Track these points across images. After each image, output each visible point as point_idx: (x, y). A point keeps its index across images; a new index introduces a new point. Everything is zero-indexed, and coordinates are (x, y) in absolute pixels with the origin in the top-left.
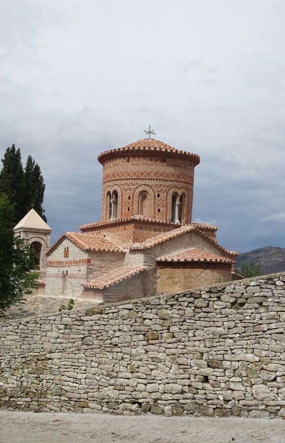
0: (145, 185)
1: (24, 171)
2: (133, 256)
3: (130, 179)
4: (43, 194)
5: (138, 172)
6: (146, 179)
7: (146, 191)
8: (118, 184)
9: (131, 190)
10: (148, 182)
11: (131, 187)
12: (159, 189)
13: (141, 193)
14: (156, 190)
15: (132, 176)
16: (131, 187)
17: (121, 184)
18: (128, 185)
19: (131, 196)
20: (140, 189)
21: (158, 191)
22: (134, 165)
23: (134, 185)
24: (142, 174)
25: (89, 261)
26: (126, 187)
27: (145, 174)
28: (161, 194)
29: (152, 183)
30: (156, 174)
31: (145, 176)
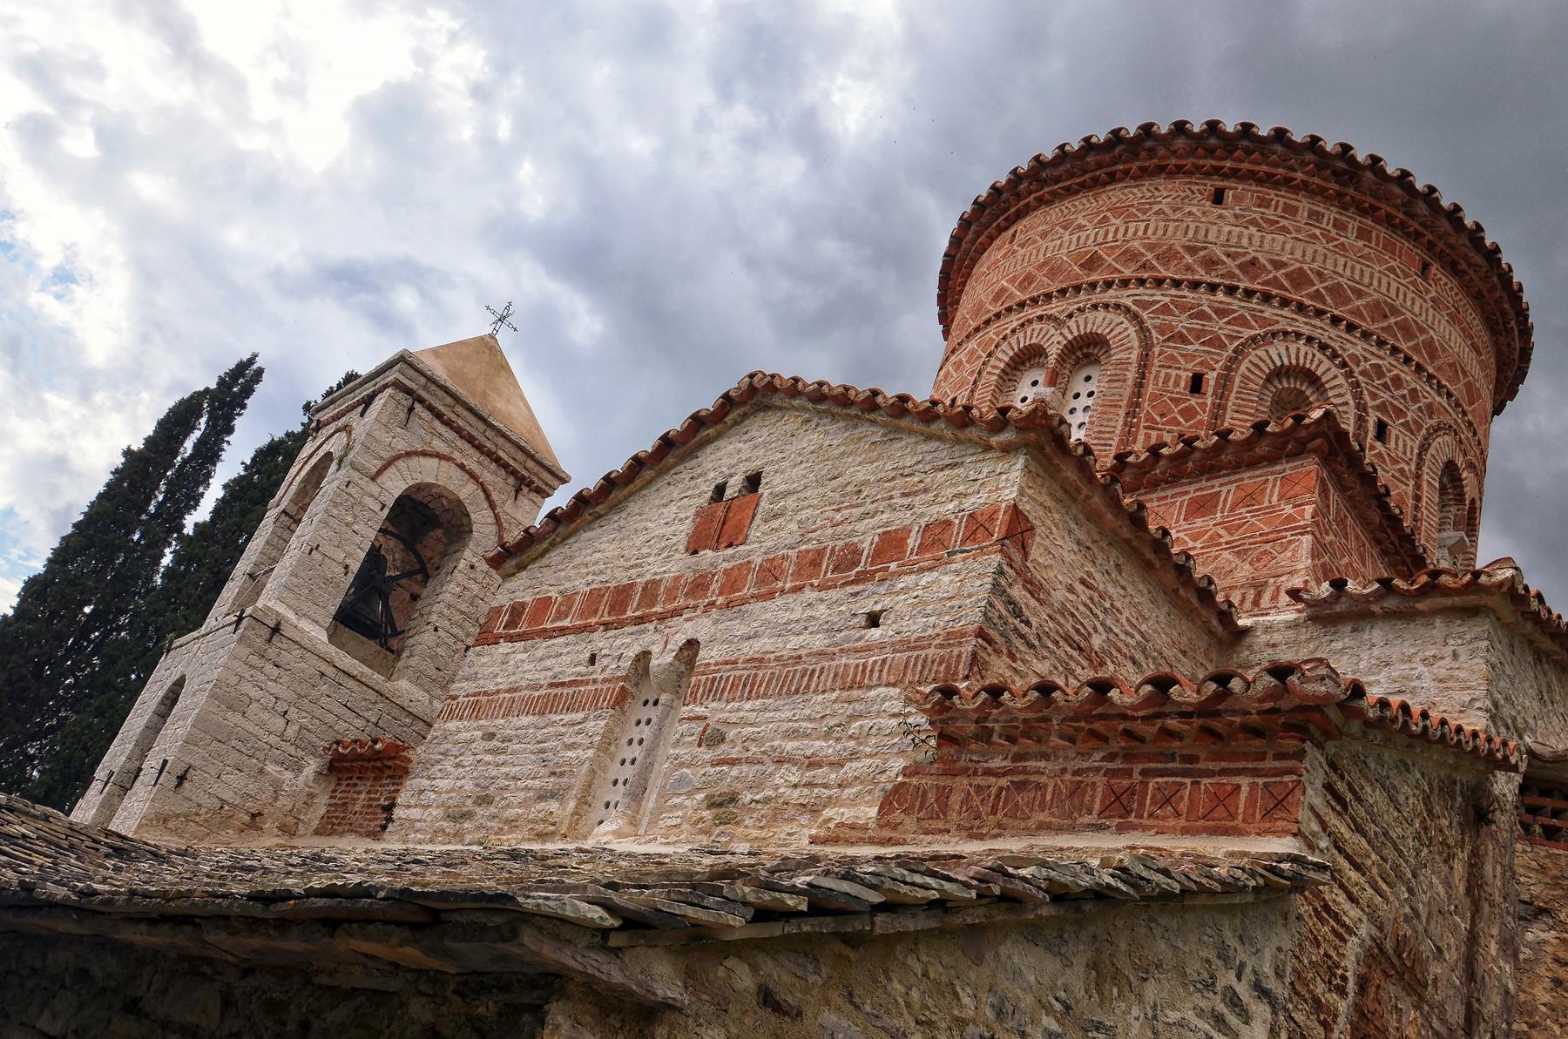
0: (1310, 340)
1: (158, 580)
2: (565, 466)
3: (1213, 288)
4: (61, 557)
5: (1278, 265)
6: (1319, 313)
7: (1312, 378)
8: (1128, 302)
9: (1216, 342)
10: (1330, 334)
11: (1220, 327)
12: (1386, 396)
13: (1279, 373)
14: (1374, 396)
15: (1231, 275)
16: (1220, 327)
17: (1144, 305)
18: (1201, 315)
19: (1211, 377)
20: (1279, 353)
21: (1382, 408)
22: (1253, 222)
23: (1242, 321)
24: (1299, 279)
25: (1018, 529)
26: (1182, 323)
27: (1320, 286)
28: (1394, 431)
29: (1358, 348)
30: (1380, 310)
31: (1317, 296)
